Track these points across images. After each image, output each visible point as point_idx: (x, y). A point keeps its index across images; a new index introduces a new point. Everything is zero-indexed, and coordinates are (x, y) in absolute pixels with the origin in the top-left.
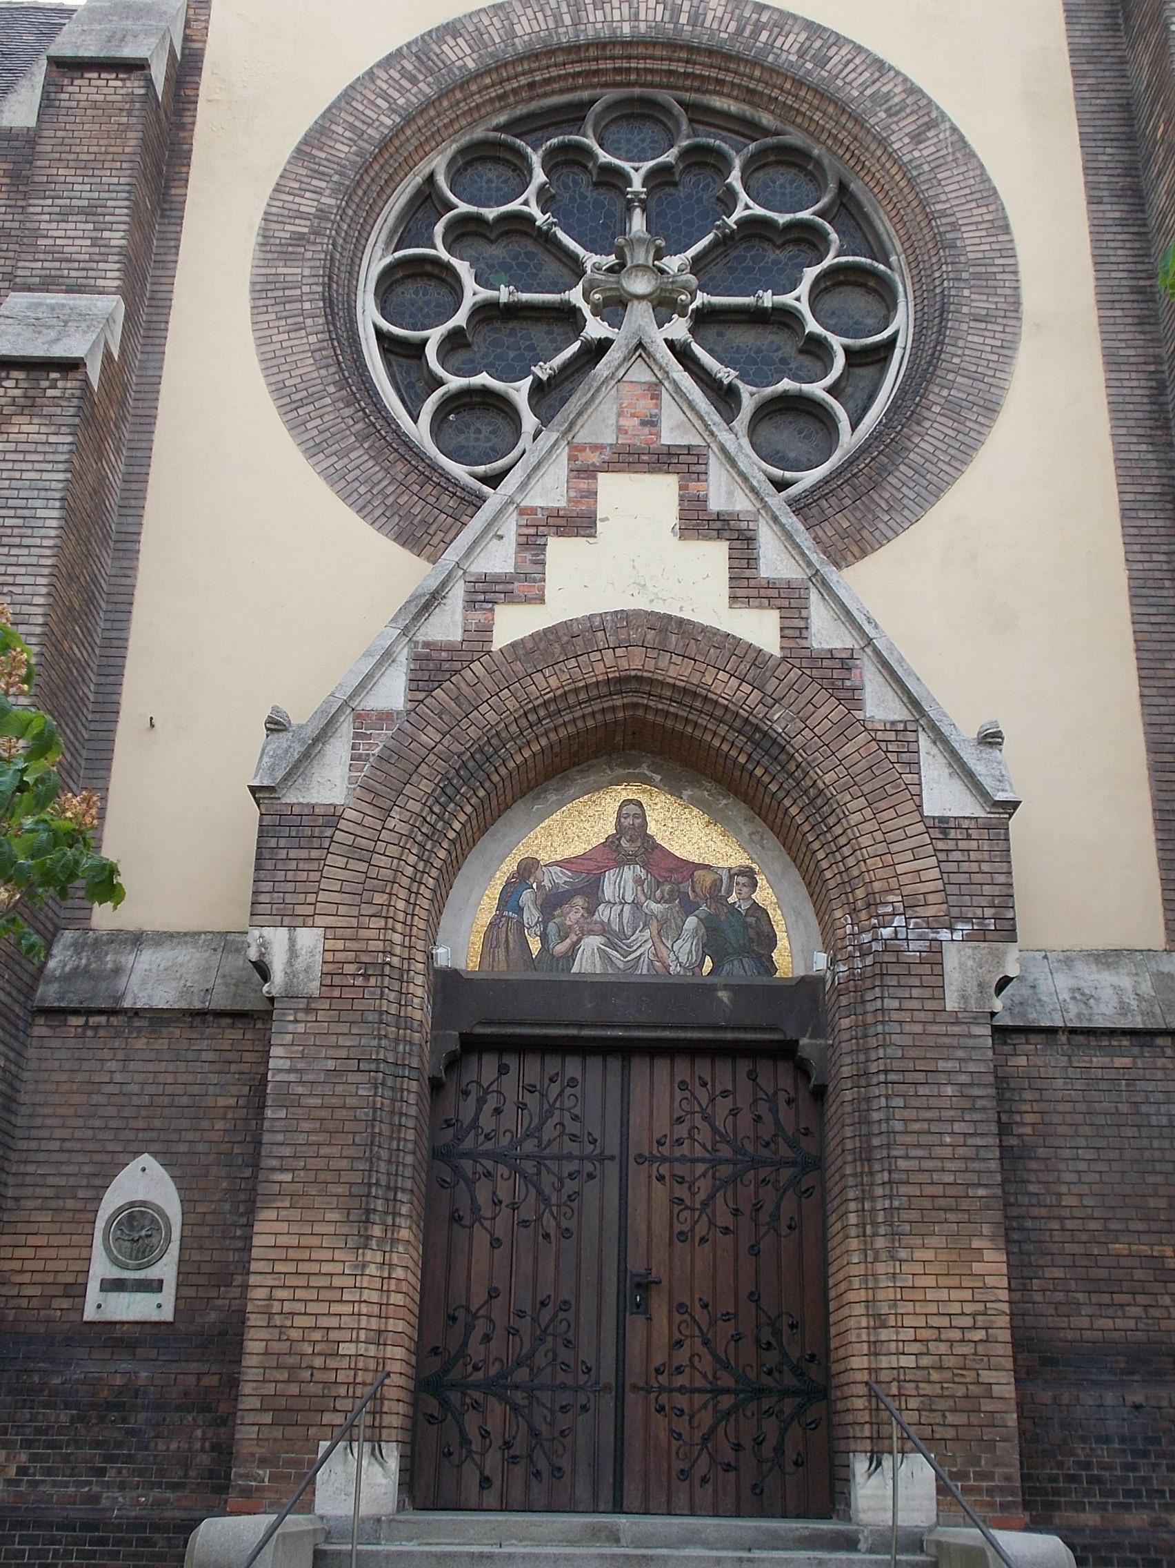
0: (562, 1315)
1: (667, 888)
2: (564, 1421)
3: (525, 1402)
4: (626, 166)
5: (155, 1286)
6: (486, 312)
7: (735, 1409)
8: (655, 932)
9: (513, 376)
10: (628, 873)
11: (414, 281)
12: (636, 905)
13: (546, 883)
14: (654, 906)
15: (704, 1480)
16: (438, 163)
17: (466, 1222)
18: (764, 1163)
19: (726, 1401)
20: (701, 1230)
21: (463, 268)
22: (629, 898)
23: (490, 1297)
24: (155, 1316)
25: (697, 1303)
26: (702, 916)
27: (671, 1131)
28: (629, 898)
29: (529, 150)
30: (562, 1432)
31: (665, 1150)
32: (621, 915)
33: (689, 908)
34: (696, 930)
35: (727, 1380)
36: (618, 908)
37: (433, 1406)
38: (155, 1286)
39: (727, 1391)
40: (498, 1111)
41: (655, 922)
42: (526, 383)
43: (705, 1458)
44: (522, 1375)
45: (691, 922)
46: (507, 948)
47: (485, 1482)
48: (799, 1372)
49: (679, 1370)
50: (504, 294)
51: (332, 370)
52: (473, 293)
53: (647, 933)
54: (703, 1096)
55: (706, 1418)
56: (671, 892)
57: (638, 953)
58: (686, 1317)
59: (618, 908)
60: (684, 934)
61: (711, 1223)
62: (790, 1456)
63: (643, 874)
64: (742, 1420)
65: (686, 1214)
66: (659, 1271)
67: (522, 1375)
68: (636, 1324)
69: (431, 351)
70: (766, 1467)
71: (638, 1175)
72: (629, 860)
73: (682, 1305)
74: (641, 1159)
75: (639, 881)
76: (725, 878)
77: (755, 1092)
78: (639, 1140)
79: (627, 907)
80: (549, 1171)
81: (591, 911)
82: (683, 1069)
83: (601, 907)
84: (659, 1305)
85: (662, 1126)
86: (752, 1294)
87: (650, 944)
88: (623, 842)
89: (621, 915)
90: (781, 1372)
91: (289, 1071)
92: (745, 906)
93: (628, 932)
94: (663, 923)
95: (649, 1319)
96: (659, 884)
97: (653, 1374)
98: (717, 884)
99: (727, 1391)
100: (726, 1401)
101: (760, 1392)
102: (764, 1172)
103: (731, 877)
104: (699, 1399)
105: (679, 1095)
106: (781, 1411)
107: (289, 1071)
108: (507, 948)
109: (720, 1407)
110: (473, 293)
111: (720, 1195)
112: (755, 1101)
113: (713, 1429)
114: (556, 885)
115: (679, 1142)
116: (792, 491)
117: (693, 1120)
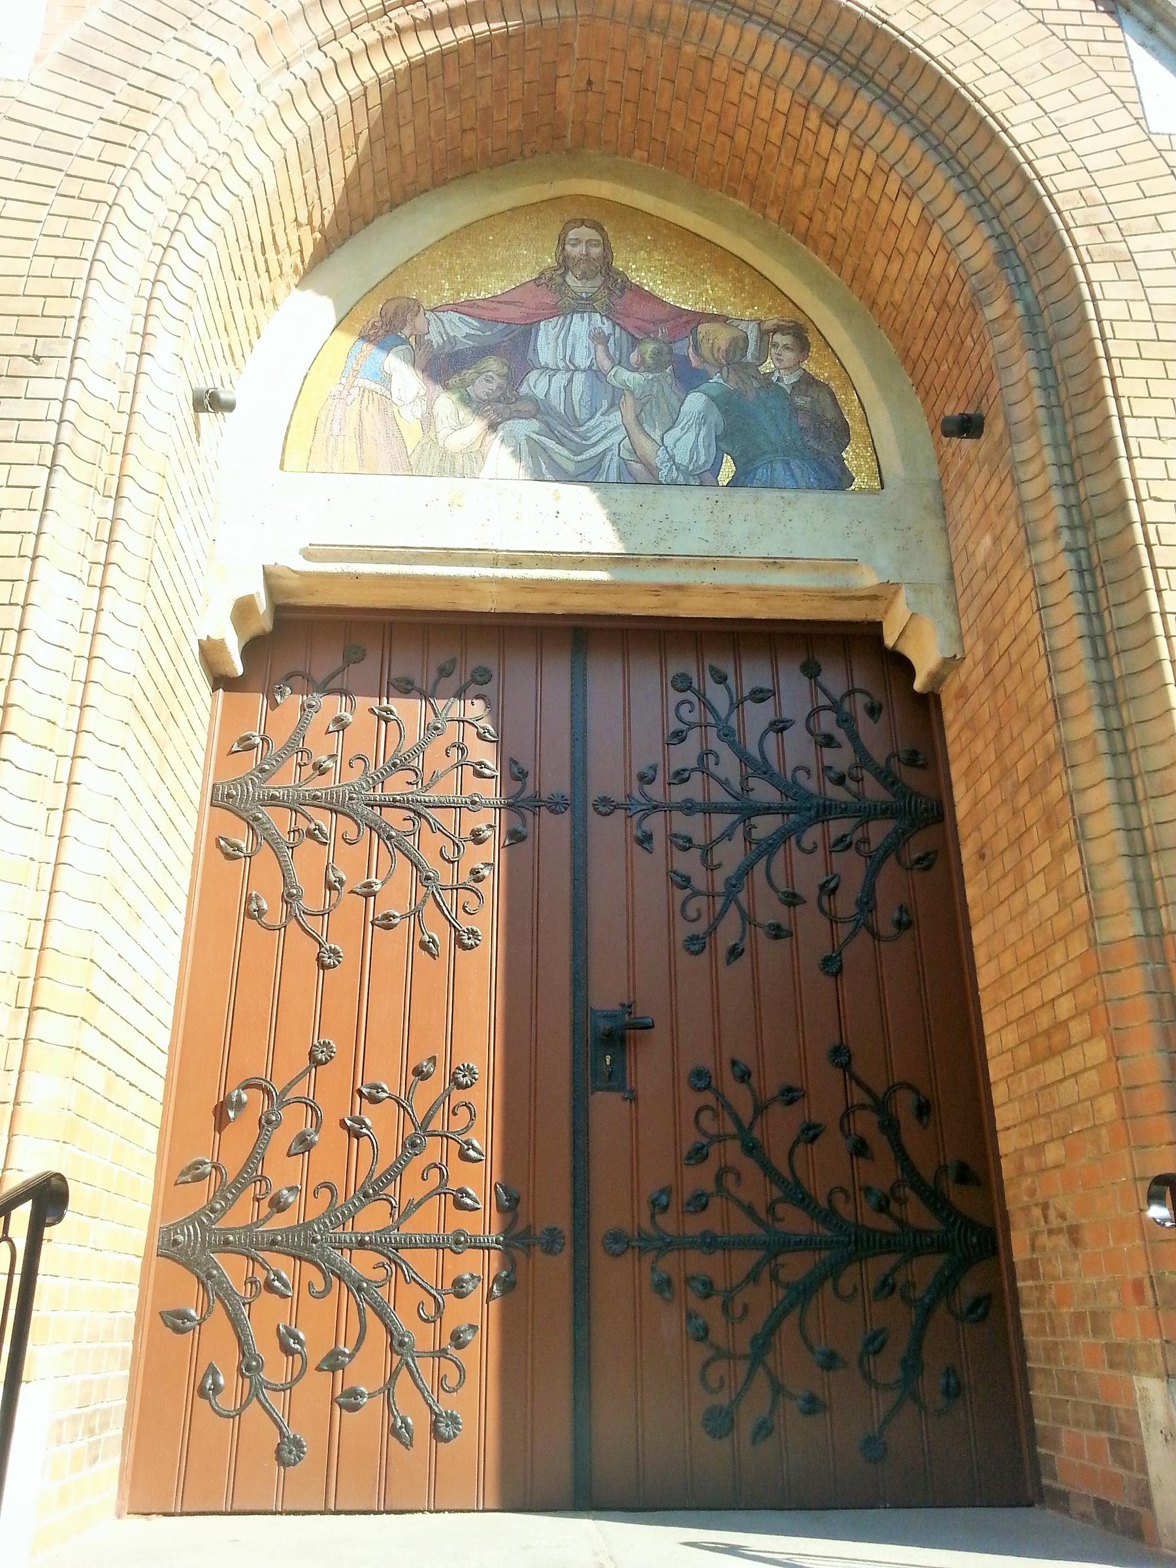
0: (458, 1096)
1: (649, 348)
3: (409, 826)
7: (782, 837)
8: (630, 417)
10: (580, 326)
12: (595, 373)
13: (435, 338)
14: (626, 375)
15: (735, 953)
17: (228, 1401)
18: (844, 811)
19: (765, 826)
20: (729, 932)
22: (582, 361)
23: (315, 1062)
25: (727, 1066)
26: (714, 393)
27: (666, 757)
28: (582, 361)
30: (458, 1282)
31: (655, 791)
32: (568, 388)
33: (689, 379)
34: (703, 420)
35: (763, 792)
36: (560, 379)
37: (188, 1296)
39: (768, 810)
40: (304, 1144)
41: (630, 400)
43: (733, 919)
44: (397, 785)
45: (695, 402)
46: (360, 436)
47: (287, 1452)
48: (934, 1199)
49: (681, 777)
53: (615, 418)
54: (718, 696)
55: (731, 854)
56: (657, 354)
57: (600, 448)
58: (689, 695)
59: (560, 379)
60: (683, 419)
61: (748, 919)
62: (885, 919)
63: (607, 327)
64: (797, 854)
65: (700, 902)
66: (649, 1008)
67: (373, 1219)
68: (606, 1106)
70: (844, 930)
71: (609, 834)
72: (584, 305)
73: (699, 1074)
74: (607, 806)
75: (599, 338)
76: (752, 336)
77: (813, 697)
78: (607, 779)
79: (579, 378)
80: (436, 828)
81: (514, 378)
82: (682, 664)
83: (533, 376)
84: (650, 1067)
85: (648, 750)
86: (826, 961)
87: (622, 433)
88: (570, 279)
89: (568, 388)
90: (858, 780)
92: (789, 380)
93: (582, 414)
94: (643, 403)
95: (633, 1098)
96: (635, 342)
97: (636, 783)
98: (739, 344)
99: (768, 810)
100: (765, 826)
101: (825, 811)
102: (838, 827)
103: (764, 334)
104: (721, 822)
105: (675, 697)
106: (866, 840)
108: (360, 436)
109: (756, 834)
111: (761, 866)
112: (848, 1112)
113: (746, 870)
114: (452, 340)
115: (681, 777)
117: (704, 738)
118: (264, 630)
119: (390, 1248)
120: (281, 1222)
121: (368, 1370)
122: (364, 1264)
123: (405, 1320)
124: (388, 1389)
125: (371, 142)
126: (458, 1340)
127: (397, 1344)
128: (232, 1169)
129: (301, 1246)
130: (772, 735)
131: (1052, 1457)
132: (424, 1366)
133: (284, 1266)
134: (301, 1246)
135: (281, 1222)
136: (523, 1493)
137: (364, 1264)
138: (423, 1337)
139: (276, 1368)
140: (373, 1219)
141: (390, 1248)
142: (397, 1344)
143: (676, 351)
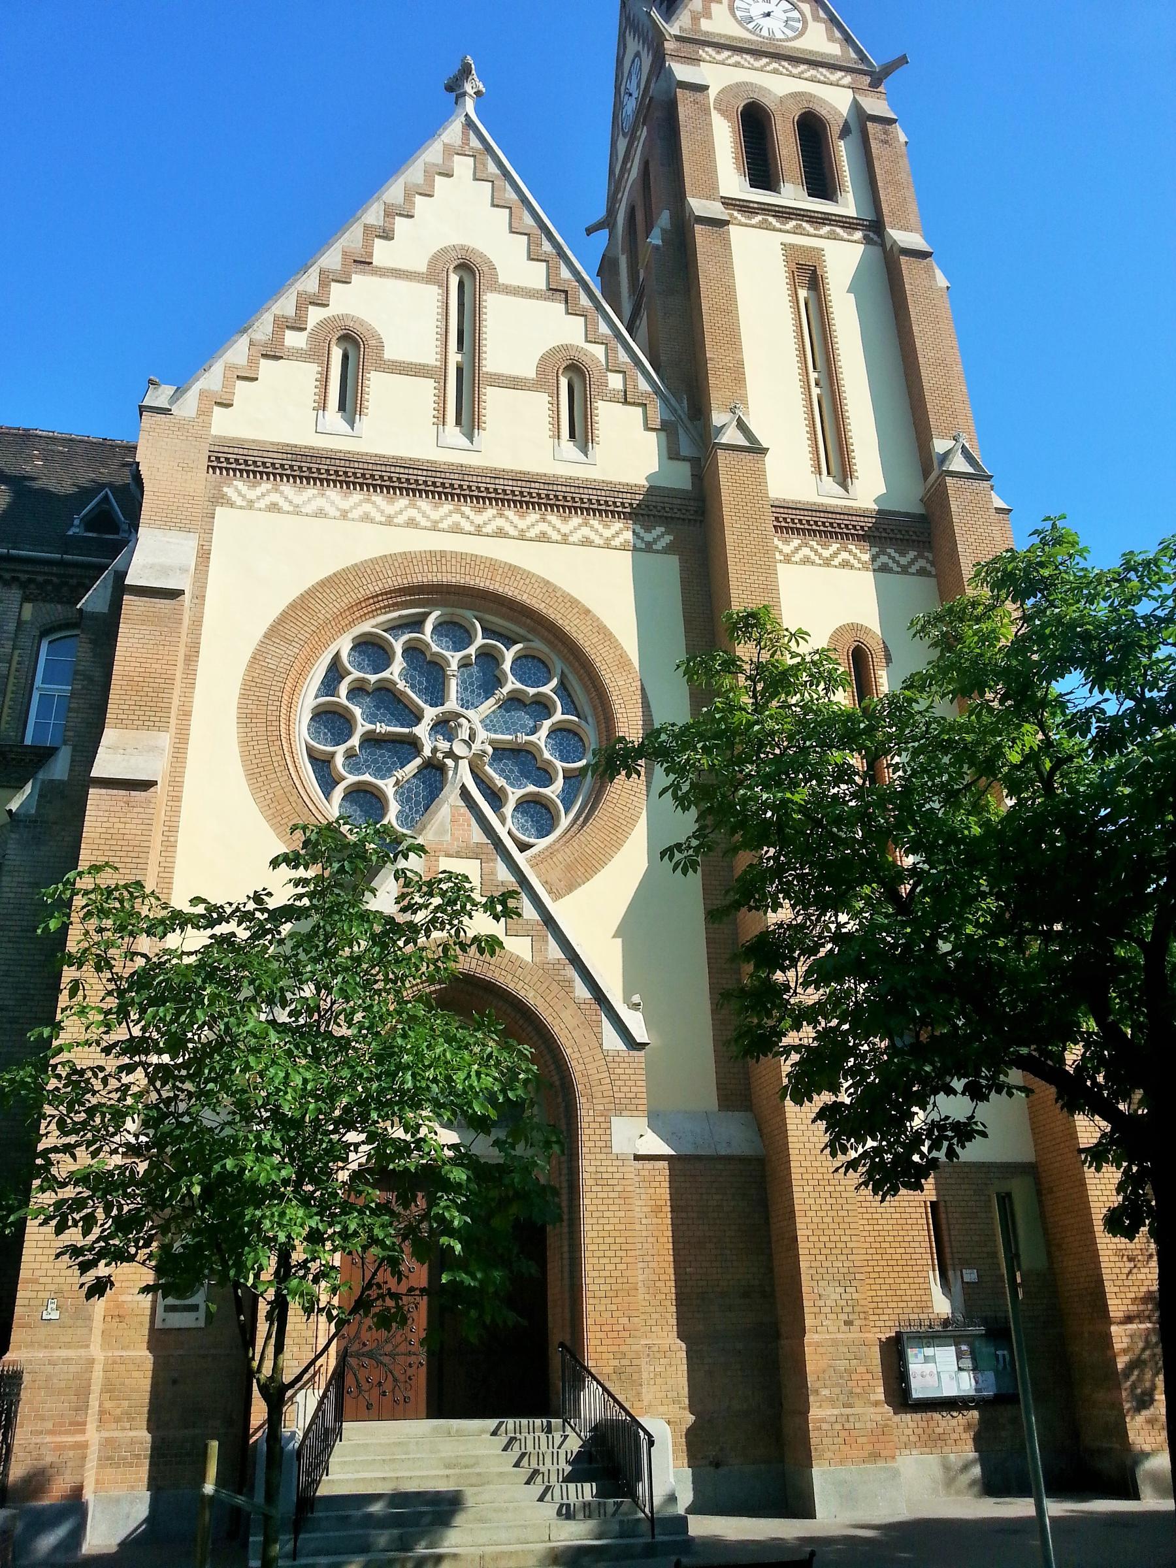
2: (410, 1372)
4: (447, 654)
5: (194, 1308)
6: (370, 740)
9: (383, 773)
11: (333, 721)
16: (344, 644)
21: (357, 711)
24: (193, 1324)
29: (392, 640)
38: (194, 1308)
42: (393, 780)
50: (381, 728)
51: (922, 1233)
52: (362, 726)
67: (388, 1348)
69: (339, 760)
91: (632, 139)
107: (632, 139)
110: (362, 726)
116: (533, 851)
118: (381, 347)
119: (392, 1355)
120: (366, 1349)
121: (388, 1386)
122: (386, 1360)
123: (396, 1374)
124: (393, 1391)
125: (333, 1374)
126: (410, 1379)
127: (395, 1380)
128: (352, 1335)
129: (370, 1355)
130: (571, 539)
131: (995, 1484)
132: (402, 1385)
133: (366, 1361)
134: (370, 1355)
135: (366, 1349)
136: (431, 1415)
137: (386, 1360)
138: (402, 1378)
139: (365, 1386)
140: (388, 1348)
141: (392, 1355)
142: (395, 1380)
143: (1125, 1345)
